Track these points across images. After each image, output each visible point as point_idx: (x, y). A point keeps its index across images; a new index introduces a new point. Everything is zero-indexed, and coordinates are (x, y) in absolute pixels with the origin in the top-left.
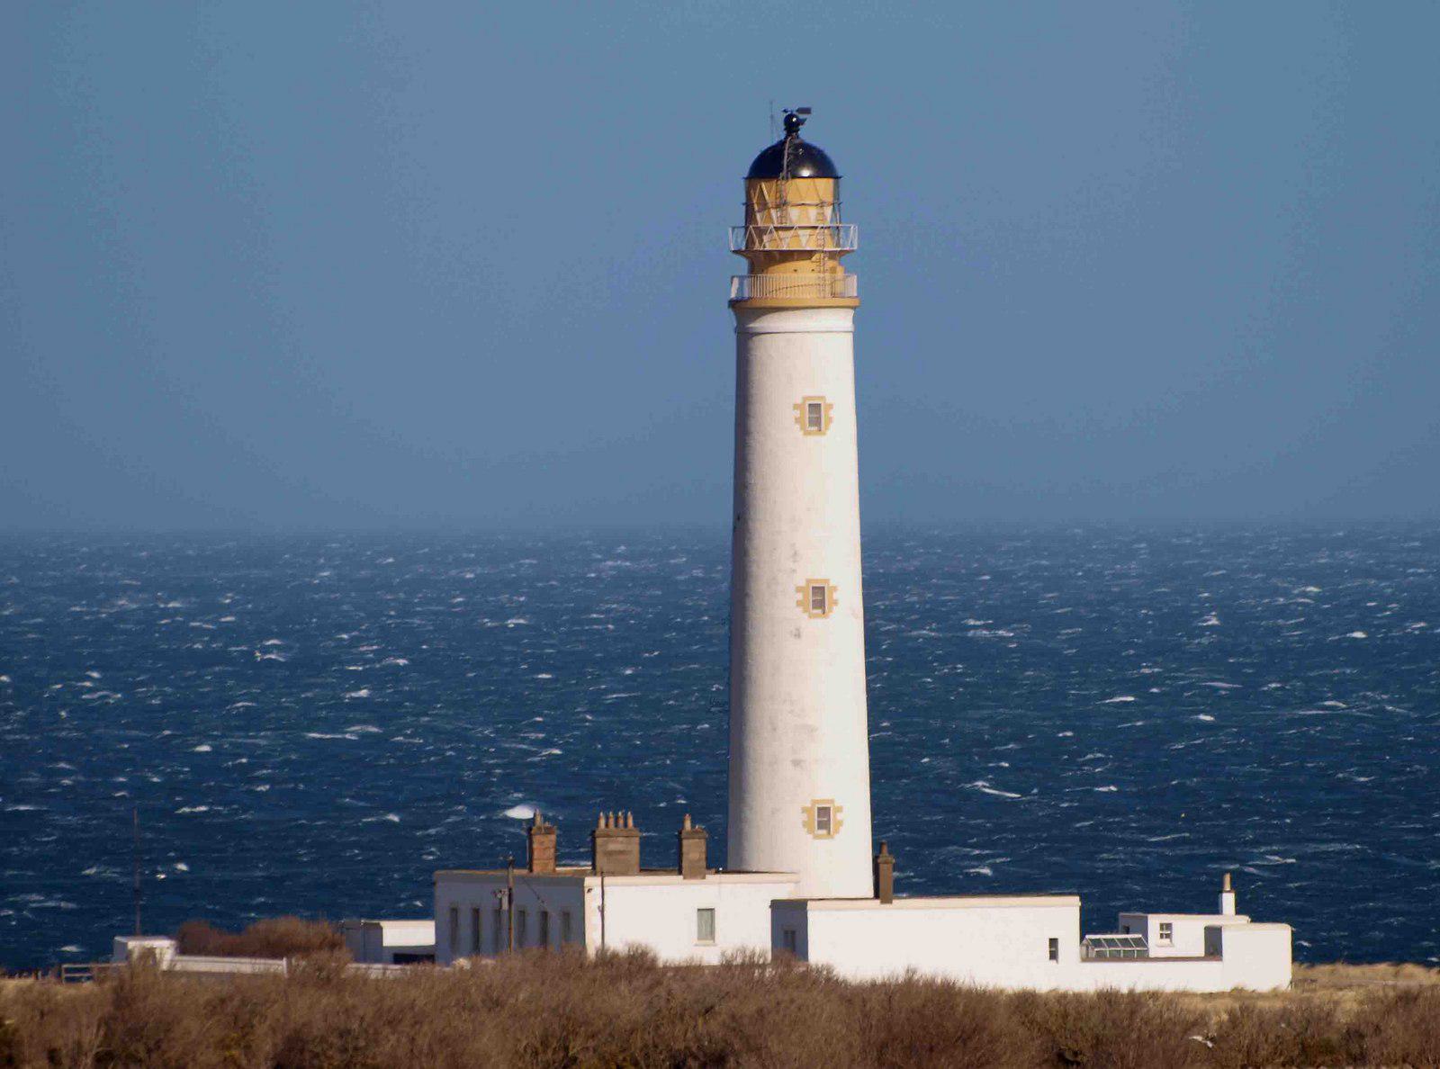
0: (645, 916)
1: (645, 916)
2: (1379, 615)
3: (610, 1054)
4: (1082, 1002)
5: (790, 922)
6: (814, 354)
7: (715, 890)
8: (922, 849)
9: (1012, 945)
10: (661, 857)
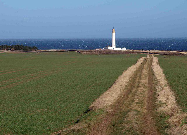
0: (109, 48)
1: (109, 48)
2: (42, 51)
3: (125, 89)
4: (154, 76)
5: (113, 48)
6: (114, 34)
7: (111, 47)
8: (116, 47)
9: (119, 49)
10: (110, 47)
